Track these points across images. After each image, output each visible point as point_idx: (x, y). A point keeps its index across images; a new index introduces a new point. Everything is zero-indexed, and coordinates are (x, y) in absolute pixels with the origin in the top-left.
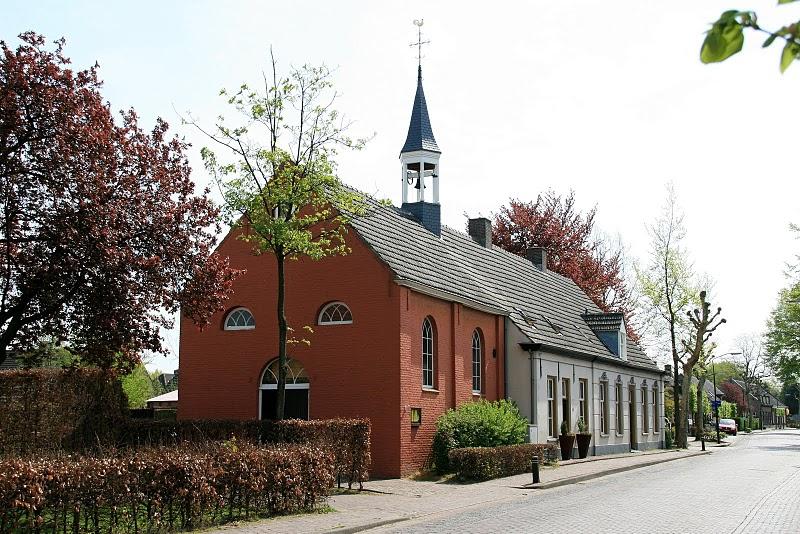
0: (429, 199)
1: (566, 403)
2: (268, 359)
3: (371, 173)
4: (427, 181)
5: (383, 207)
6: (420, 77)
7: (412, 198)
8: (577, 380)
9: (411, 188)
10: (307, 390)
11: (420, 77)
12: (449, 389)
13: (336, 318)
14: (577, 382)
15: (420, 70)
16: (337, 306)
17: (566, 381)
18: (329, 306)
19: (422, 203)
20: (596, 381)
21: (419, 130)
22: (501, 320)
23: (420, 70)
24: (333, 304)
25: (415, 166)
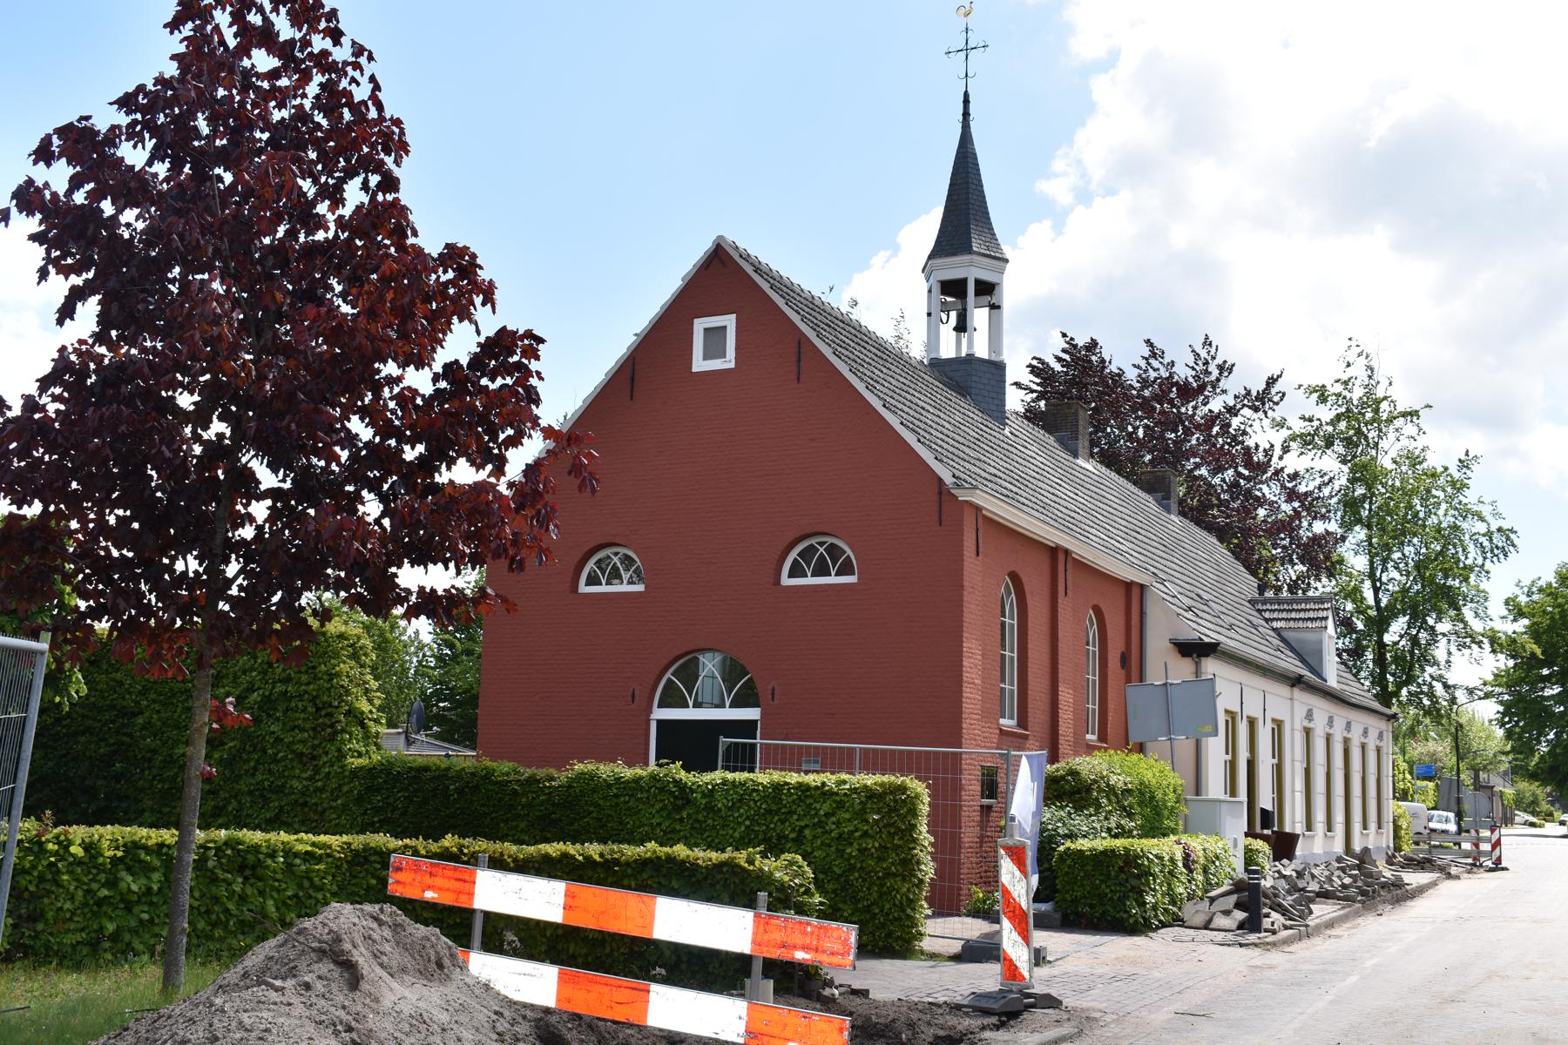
0: (982, 351)
1: (1251, 764)
2: (672, 656)
3: (885, 294)
4: (979, 317)
5: (885, 354)
6: (966, 114)
7: (948, 348)
8: (1268, 720)
9: (947, 332)
10: (756, 722)
11: (966, 114)
12: (1245, 669)
13: (822, 570)
14: (1269, 725)
15: (966, 101)
16: (821, 544)
17: (1252, 722)
18: (601, 555)
19: (971, 358)
20: (1298, 726)
21: (965, 217)
22: (1135, 592)
23: (966, 101)
24: (813, 541)
25: (954, 288)
